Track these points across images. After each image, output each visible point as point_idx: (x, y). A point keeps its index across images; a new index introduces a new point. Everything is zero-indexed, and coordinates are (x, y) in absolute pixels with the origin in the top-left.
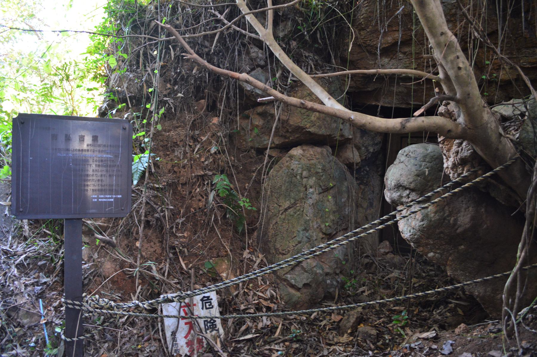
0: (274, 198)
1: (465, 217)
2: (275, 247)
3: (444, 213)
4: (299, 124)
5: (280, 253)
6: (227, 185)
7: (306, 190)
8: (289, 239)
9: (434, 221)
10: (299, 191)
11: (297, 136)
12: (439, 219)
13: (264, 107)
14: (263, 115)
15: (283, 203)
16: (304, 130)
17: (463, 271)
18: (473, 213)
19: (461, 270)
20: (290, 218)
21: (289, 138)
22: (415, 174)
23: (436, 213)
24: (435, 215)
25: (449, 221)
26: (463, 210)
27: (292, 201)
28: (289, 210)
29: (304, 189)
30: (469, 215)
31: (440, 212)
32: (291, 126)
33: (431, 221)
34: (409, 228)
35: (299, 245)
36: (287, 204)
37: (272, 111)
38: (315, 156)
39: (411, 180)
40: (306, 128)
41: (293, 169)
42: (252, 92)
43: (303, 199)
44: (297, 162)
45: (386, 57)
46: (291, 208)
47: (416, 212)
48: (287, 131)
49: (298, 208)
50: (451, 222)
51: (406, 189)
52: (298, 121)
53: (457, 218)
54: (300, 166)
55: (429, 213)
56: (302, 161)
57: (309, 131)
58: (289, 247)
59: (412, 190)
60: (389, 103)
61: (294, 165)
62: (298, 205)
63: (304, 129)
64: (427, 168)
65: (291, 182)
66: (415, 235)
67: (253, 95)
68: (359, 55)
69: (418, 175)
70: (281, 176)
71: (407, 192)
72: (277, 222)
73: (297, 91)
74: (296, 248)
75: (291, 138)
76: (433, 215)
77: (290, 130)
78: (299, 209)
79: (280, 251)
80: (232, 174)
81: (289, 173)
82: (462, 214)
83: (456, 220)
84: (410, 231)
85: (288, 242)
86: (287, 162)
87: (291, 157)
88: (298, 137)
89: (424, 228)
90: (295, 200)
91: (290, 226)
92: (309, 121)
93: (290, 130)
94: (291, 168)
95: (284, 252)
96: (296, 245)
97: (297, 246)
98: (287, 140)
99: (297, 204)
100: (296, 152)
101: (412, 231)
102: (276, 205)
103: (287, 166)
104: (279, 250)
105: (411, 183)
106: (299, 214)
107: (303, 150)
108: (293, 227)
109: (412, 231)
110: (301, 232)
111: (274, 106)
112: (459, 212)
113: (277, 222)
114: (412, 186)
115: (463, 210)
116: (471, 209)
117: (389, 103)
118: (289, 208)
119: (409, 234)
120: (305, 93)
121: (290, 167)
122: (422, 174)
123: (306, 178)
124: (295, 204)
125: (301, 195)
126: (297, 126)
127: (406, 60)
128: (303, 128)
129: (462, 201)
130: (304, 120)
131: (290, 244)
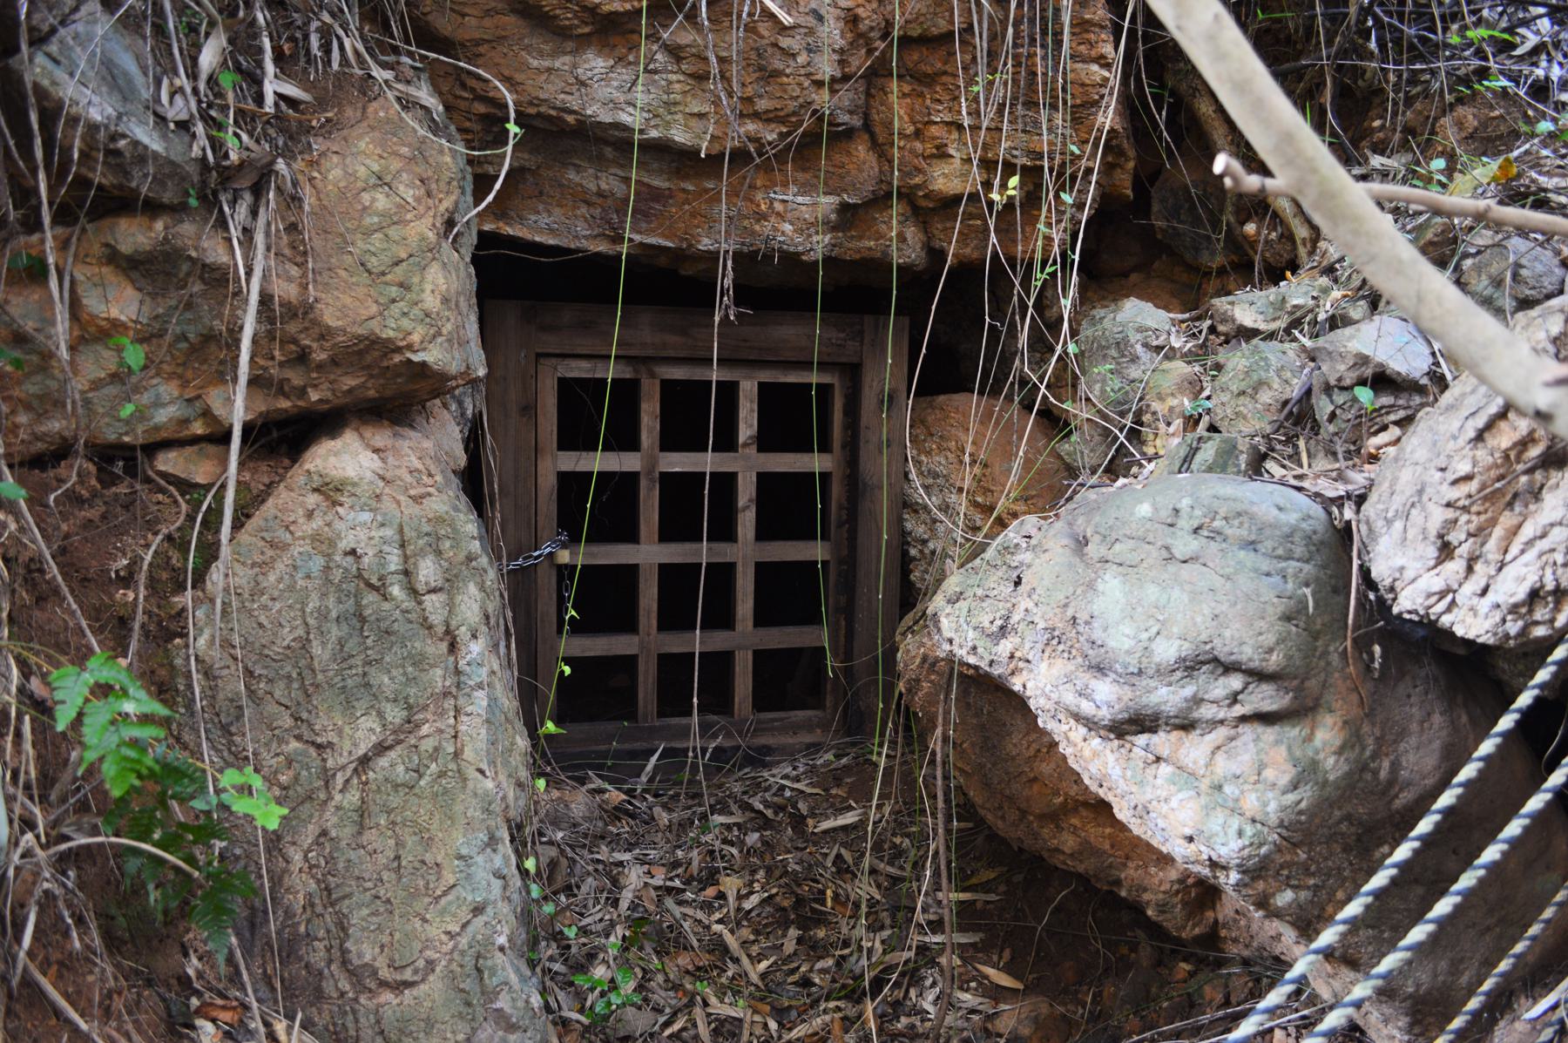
0: (272, 708)
1: (1421, 753)
2: (345, 963)
3: (1363, 749)
4: (374, 325)
5: (384, 984)
6: (146, 719)
7: (453, 647)
8: (419, 906)
9: (1335, 782)
10: (419, 661)
11: (349, 382)
12: (1348, 775)
13: (159, 225)
14: (152, 270)
15: (340, 732)
16: (397, 358)
17: (1373, 927)
18: (1444, 733)
19: (1368, 927)
20: (395, 801)
21: (302, 392)
22: (1280, 609)
23: (1340, 752)
24: (1337, 761)
25: (1376, 773)
26: (1414, 727)
27: (395, 715)
28: (383, 762)
29: (444, 646)
30: (1437, 744)
31: (1353, 747)
32: (325, 334)
33: (1325, 783)
34: (1235, 823)
35: (480, 920)
36: (366, 732)
37: (215, 253)
38: (430, 475)
39: (1269, 639)
40: (410, 347)
41: (353, 552)
42: (114, 137)
43: (446, 694)
44: (366, 516)
45: (599, 54)
46: (390, 748)
47: (429, 592)
48: (302, 358)
49: (428, 745)
50: (1383, 774)
51: (1229, 668)
52: (365, 314)
53: (1397, 758)
54: (389, 532)
55: (1321, 756)
56: (387, 504)
57: (424, 364)
58: (427, 944)
59: (1259, 676)
60: (552, 231)
61: (357, 529)
62: (425, 729)
63: (399, 350)
64: (1307, 585)
65: (363, 620)
66: (1261, 845)
67: (117, 153)
68: (487, 22)
69: (1287, 618)
70: (291, 588)
71: (1236, 682)
72: (324, 833)
73: (322, 154)
74: (464, 942)
75: (314, 396)
76: (1331, 760)
77: (320, 356)
78: (436, 749)
79: (385, 973)
80: (81, 628)
81: (337, 575)
82: (1413, 741)
83: (1395, 766)
84: (1240, 834)
85: (418, 923)
86: (310, 515)
87: (331, 491)
88: (350, 391)
89: (1300, 813)
90: (409, 708)
91: (410, 841)
92: (416, 311)
93: (320, 356)
94: (344, 545)
95: (408, 975)
96: (464, 926)
97: (470, 929)
98: (284, 404)
99: (418, 726)
100: (346, 457)
101: (1249, 830)
102: (294, 745)
103: (316, 538)
104: (375, 972)
105: (1270, 651)
106: (442, 774)
107: (376, 451)
108: (428, 843)
109: (1249, 830)
110: (480, 859)
111: (222, 223)
112: (1403, 734)
113: (324, 833)
114: (1275, 661)
115: (1414, 727)
116: (1437, 719)
117: (552, 231)
118: (381, 749)
119: (1235, 844)
120: (362, 172)
121: (332, 543)
122: (1299, 612)
123: (434, 591)
124: (411, 725)
125: (438, 678)
126: (360, 338)
127: (674, 77)
128: (389, 347)
129: (1409, 696)
130: (395, 310)
131: (434, 931)
